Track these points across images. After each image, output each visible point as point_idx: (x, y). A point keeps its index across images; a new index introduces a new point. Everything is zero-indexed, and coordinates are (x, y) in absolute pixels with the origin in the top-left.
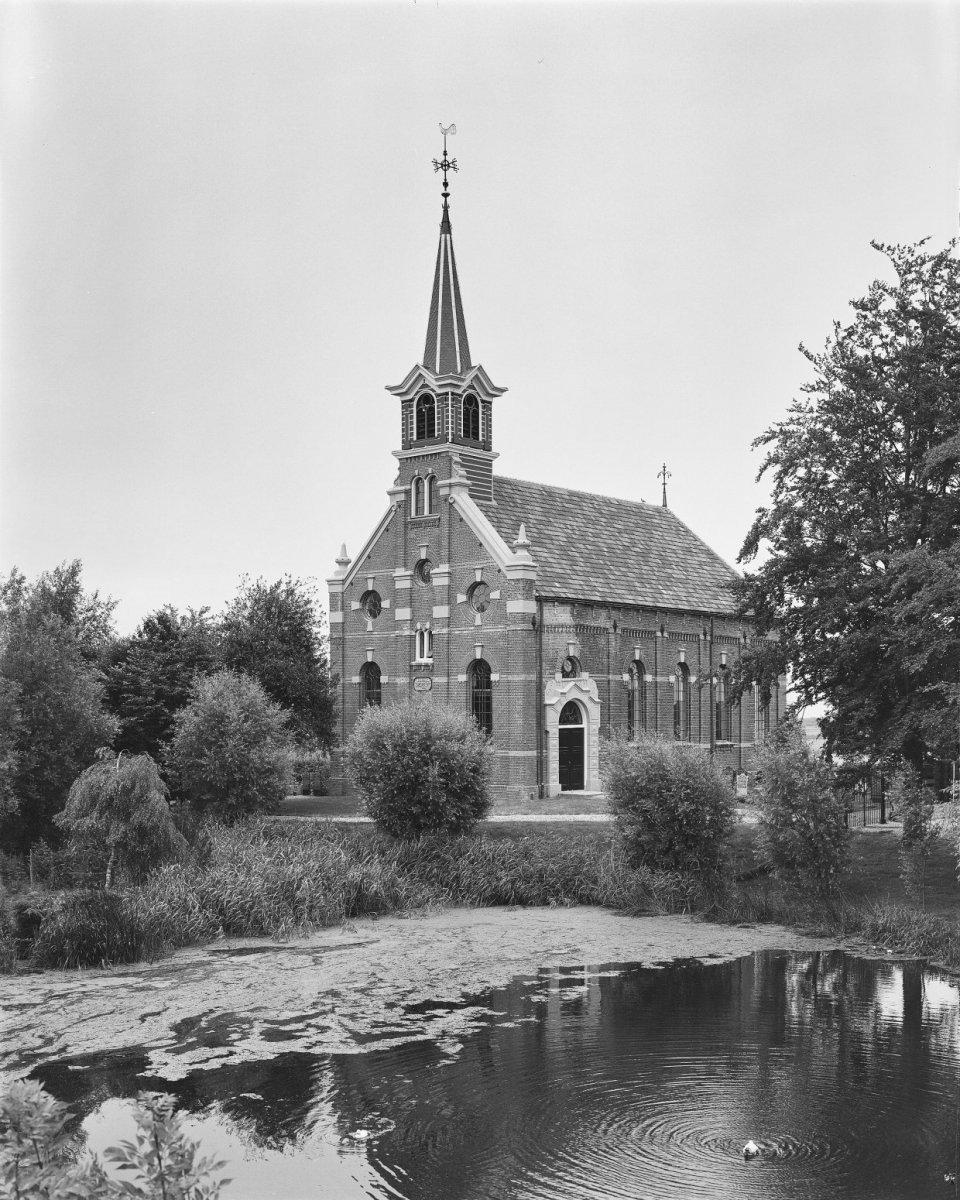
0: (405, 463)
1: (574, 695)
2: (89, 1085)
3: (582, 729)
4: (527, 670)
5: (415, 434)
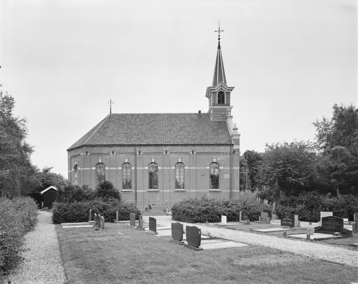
2: (329, 167)
4: (233, 170)
5: (217, 102)
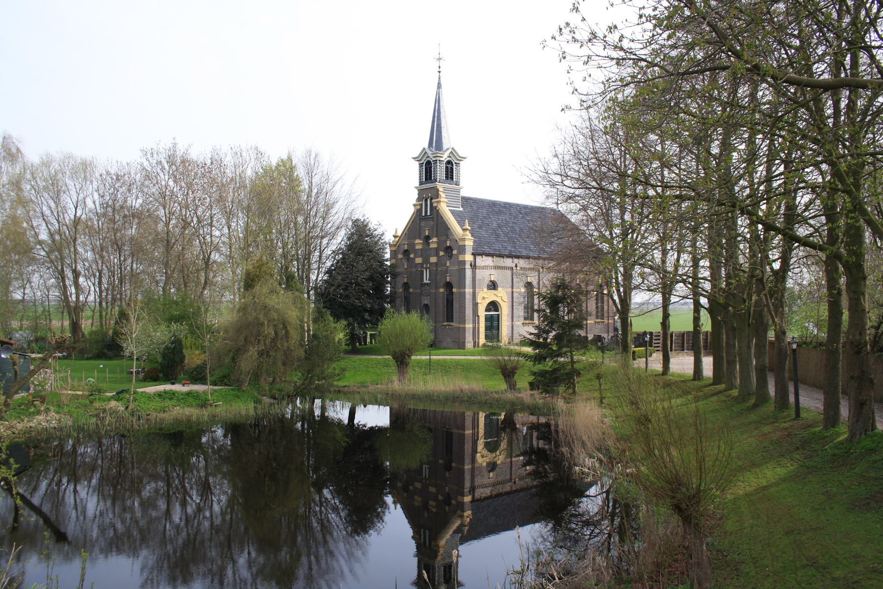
0: (421, 192)
1: (494, 298)
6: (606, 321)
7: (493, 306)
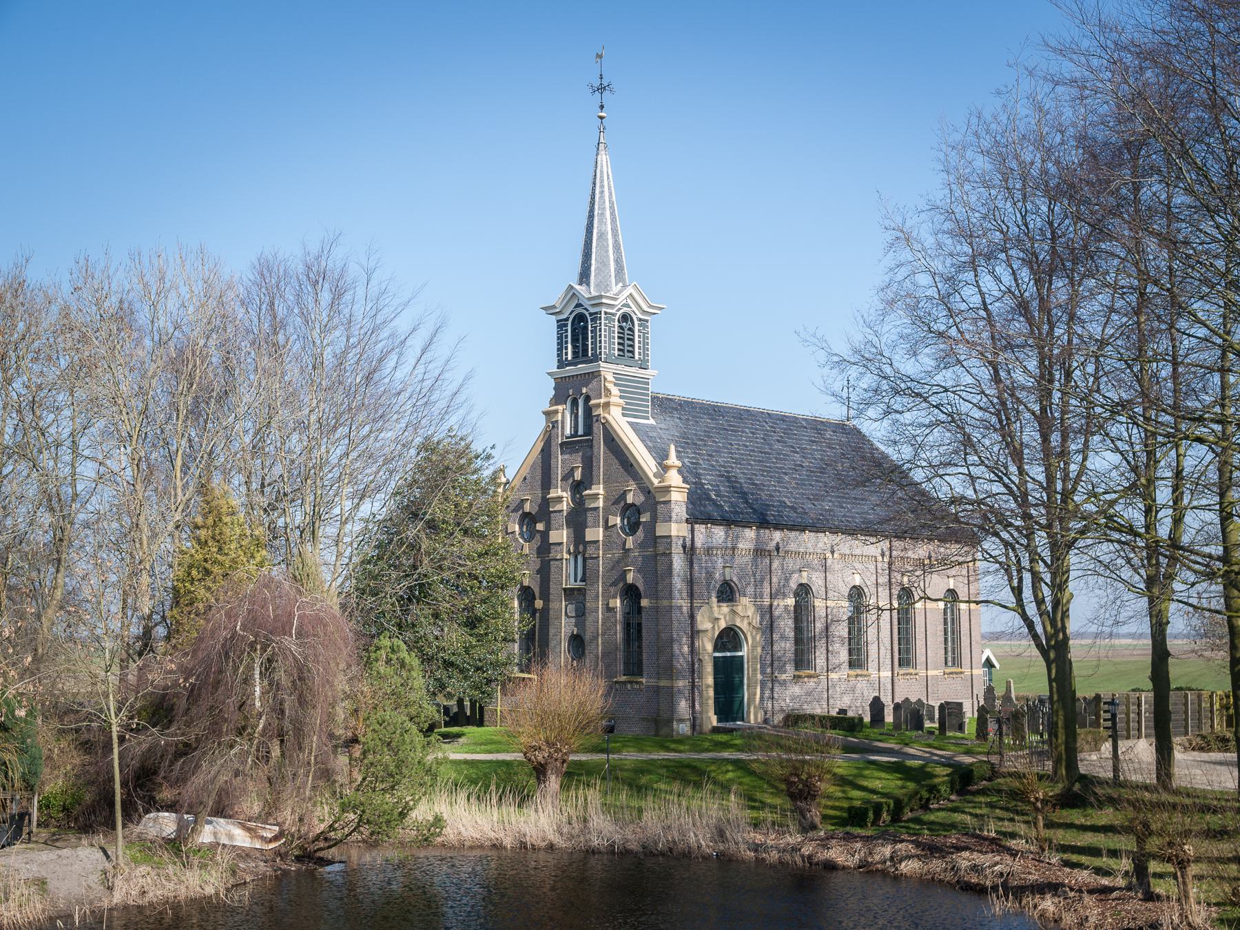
3: (742, 657)
6: (923, 673)
7: (729, 638)
